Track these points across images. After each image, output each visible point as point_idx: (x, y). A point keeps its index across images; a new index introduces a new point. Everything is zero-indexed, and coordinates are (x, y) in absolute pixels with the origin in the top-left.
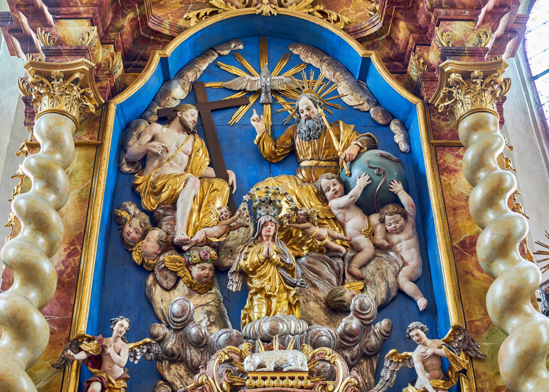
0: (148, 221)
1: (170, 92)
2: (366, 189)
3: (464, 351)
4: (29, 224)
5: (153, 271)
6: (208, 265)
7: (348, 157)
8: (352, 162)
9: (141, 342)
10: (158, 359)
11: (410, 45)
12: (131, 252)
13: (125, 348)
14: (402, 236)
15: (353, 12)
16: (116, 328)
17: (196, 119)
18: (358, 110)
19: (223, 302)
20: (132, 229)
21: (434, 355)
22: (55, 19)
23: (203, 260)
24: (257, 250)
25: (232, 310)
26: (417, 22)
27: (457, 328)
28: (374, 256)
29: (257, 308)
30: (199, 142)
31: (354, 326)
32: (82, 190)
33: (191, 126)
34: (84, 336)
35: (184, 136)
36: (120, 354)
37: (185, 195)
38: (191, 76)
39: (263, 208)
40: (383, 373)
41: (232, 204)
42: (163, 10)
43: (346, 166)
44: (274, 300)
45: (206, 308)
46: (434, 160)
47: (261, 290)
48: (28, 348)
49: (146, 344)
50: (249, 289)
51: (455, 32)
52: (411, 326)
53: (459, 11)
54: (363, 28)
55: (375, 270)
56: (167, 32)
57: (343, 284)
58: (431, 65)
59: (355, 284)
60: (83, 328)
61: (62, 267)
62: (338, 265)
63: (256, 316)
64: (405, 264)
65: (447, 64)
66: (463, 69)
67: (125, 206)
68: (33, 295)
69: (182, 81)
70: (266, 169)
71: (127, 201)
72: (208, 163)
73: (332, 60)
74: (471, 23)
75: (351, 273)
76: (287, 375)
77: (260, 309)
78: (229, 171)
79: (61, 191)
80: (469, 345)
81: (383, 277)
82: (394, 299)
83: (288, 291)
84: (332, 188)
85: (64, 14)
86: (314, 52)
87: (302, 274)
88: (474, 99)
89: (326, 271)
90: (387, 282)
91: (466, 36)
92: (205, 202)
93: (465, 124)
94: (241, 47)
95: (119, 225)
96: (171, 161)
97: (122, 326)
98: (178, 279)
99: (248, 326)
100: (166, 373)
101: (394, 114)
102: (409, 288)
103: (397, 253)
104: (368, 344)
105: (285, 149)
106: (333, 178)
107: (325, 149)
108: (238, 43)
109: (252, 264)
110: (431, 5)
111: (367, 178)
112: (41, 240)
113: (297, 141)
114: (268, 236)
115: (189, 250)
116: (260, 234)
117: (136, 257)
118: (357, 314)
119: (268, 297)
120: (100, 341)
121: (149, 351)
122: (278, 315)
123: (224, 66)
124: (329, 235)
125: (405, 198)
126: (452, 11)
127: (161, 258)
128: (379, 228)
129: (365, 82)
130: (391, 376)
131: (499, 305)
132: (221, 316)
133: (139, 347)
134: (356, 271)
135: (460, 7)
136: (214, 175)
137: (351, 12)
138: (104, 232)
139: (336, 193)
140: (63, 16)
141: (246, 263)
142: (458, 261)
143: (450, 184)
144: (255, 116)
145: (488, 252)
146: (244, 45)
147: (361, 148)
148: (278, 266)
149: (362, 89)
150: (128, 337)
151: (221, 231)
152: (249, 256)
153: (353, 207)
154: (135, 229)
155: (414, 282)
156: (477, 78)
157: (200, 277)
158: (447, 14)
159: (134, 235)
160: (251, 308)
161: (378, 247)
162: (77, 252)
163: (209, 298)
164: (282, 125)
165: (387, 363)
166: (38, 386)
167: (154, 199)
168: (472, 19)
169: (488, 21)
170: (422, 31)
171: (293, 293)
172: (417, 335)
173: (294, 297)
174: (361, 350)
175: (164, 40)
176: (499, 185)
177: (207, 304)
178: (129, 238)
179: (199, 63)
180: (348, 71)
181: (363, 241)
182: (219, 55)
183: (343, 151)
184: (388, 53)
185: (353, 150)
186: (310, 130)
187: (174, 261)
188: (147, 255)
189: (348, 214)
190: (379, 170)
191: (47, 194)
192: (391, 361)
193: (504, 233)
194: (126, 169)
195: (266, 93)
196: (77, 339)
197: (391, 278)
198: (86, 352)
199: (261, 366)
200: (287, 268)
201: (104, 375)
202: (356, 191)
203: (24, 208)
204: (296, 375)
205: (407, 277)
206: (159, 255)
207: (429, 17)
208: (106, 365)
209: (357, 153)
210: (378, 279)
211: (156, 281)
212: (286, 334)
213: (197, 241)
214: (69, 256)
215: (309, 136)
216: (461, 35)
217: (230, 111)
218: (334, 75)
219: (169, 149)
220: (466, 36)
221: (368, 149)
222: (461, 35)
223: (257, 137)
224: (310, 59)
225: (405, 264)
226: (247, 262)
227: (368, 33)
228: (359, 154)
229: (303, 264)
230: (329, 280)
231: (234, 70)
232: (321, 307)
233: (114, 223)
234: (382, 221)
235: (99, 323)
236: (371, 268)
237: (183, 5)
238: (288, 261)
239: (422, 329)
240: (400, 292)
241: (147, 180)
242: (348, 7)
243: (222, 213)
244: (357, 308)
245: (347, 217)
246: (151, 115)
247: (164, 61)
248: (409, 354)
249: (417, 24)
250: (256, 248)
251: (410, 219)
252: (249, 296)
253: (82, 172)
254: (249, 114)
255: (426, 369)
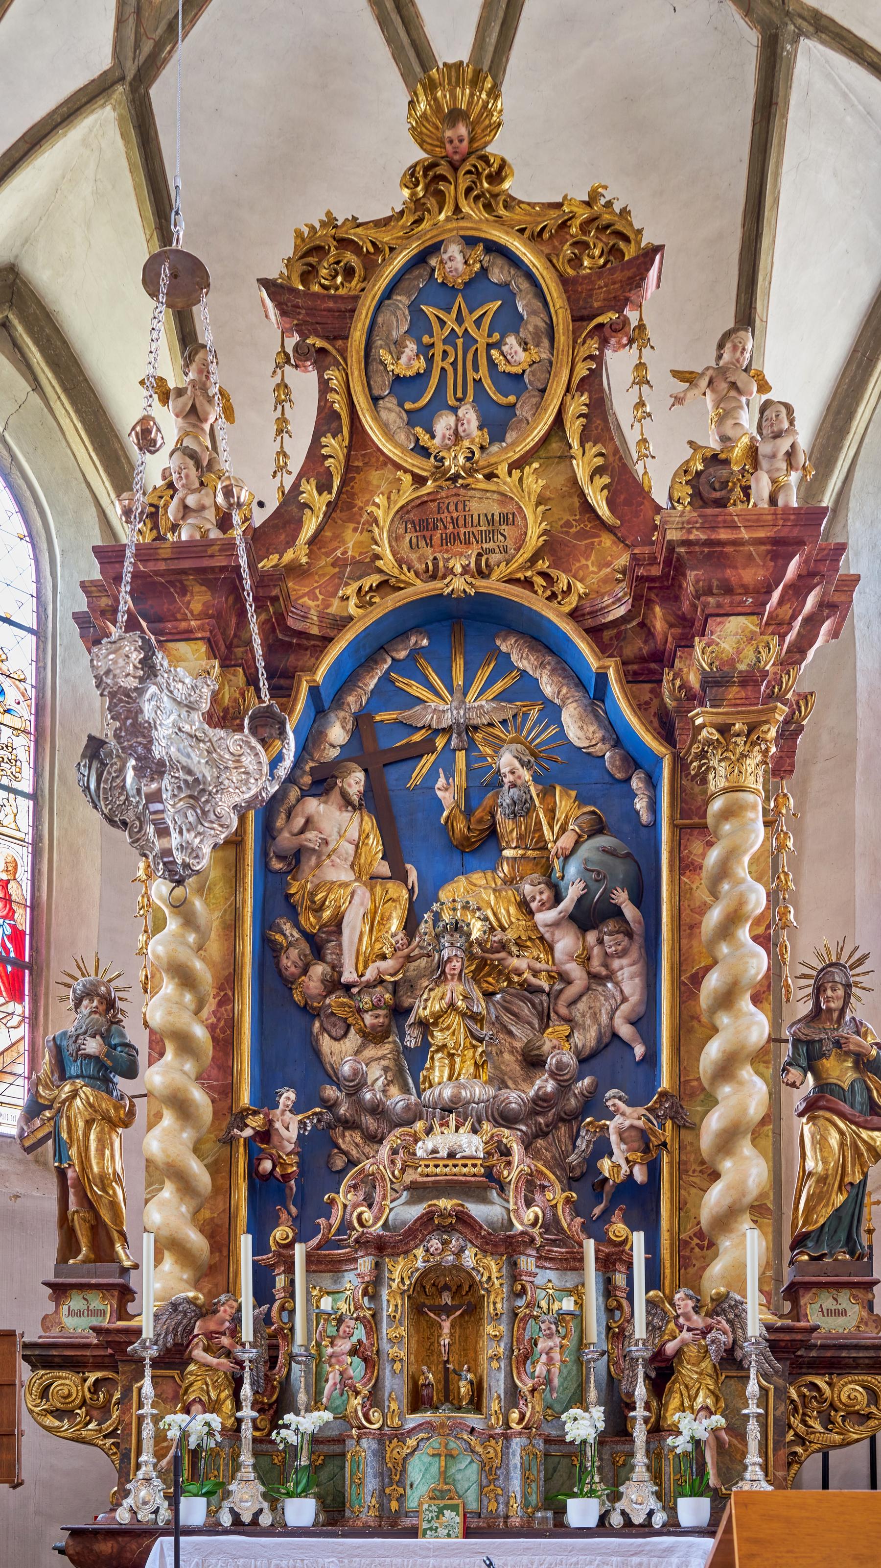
0: (308, 951)
1: (326, 735)
2: (580, 900)
3: (671, 1118)
4: (173, 978)
5: (318, 1015)
6: (382, 1012)
7: (560, 851)
8: (567, 858)
9: (310, 1113)
10: (330, 1126)
11: (668, 645)
12: (291, 989)
13: (294, 1121)
14: (625, 961)
15: (595, 569)
16: (282, 1100)
17: (362, 789)
18: (589, 754)
19: (403, 1053)
20: (290, 961)
21: (632, 1127)
22: (158, 641)
23: (375, 1007)
24: (440, 994)
25: (411, 1064)
26: (680, 609)
27: (664, 1095)
28: (588, 989)
29: (438, 1070)
30: (369, 823)
31: (549, 1089)
32: (225, 911)
33: (355, 799)
34: (248, 1109)
35: (347, 815)
36: (289, 1128)
37: (352, 916)
38: (353, 702)
39: (447, 937)
40: (579, 1142)
41: (410, 926)
42: (307, 582)
43: (557, 864)
44: (458, 1060)
45: (384, 1063)
46: (676, 850)
47: (442, 1048)
48: (193, 1127)
49: (315, 1114)
50: (430, 1045)
51: (723, 645)
52: (607, 1095)
53: (737, 598)
54: (604, 608)
55: (586, 1009)
56: (315, 631)
57: (547, 1026)
58: (691, 688)
59: (561, 1028)
60: (245, 1099)
61: (213, 1020)
62: (542, 1003)
63: (436, 1080)
64: (624, 999)
65: (698, 714)
66: (720, 720)
67: (278, 924)
68: (188, 1066)
69: (342, 714)
70: (457, 859)
71: (281, 916)
72: (380, 855)
73: (558, 663)
74: (755, 617)
75: (556, 1013)
76: (460, 1162)
77: (441, 1072)
78: (409, 866)
79: (202, 928)
80: (677, 1112)
81: (595, 1017)
82: (607, 1046)
83: (475, 1047)
84: (538, 898)
85: (170, 633)
86: (532, 649)
87: (497, 1017)
88: (729, 770)
89: (526, 1010)
90: (599, 1025)
91: (739, 652)
92: (378, 918)
93: (716, 805)
94: (425, 642)
95: (274, 951)
96: (333, 857)
97: (288, 1098)
98: (348, 1026)
99: (428, 1092)
100: (340, 1141)
101: (639, 761)
102: (625, 1031)
103: (617, 984)
104: (567, 1108)
105: (482, 831)
106: (539, 883)
107: (535, 831)
108: (420, 637)
109: (432, 1014)
110: (696, 591)
111: (582, 885)
112: (188, 997)
113: (498, 816)
114: (453, 975)
115: (359, 992)
116: (443, 972)
117: (297, 997)
118: (553, 1075)
119: (451, 1056)
120: (266, 1115)
121: (319, 1121)
122: (462, 1080)
123: (402, 682)
124: (529, 967)
125: (630, 911)
126: (727, 600)
127: (328, 1001)
128: (596, 950)
129: (603, 701)
130: (587, 1146)
131: (709, 1071)
132: (400, 1071)
133: (308, 1118)
134: (563, 1011)
135: (740, 591)
136: (389, 874)
137: (591, 569)
138: (257, 996)
139: (543, 904)
140: (170, 637)
141: (427, 1012)
142: (684, 1002)
143: (691, 889)
144: (441, 782)
145: (710, 1002)
146: (429, 639)
147: (580, 836)
148: (463, 1015)
149: (597, 716)
150: (296, 1109)
151: (398, 966)
152: (429, 1004)
153: (565, 923)
154: (294, 962)
155: (632, 1024)
156: (738, 735)
157: (373, 1026)
158: (719, 605)
159: (293, 969)
160: (432, 1068)
161: (594, 977)
162: (229, 999)
163: (386, 1049)
164: (484, 783)
165: (583, 1133)
166: (206, 1162)
167: (315, 917)
168: (756, 611)
169: (789, 600)
170: (686, 623)
171: (480, 1050)
172: (614, 1105)
173: (481, 1055)
174: (559, 1114)
175: (312, 643)
176: (736, 911)
177: (383, 1057)
178: (287, 973)
179: (364, 677)
180: (580, 684)
181: (575, 970)
182: (393, 659)
183: (555, 842)
184: (640, 649)
185: (567, 841)
186: (515, 803)
187: (343, 1005)
188: (312, 998)
189: (558, 934)
190: (599, 873)
191: (187, 935)
192: (588, 1131)
193: (729, 980)
194: (277, 865)
195: (459, 734)
196: (241, 1112)
197: (604, 1019)
198: (253, 1128)
199: (435, 1151)
200: (476, 1018)
201: (274, 1152)
202: (573, 893)
203: (165, 960)
204: (469, 1162)
205: (625, 1018)
206: (325, 997)
207: (695, 607)
208: (275, 1139)
209: (572, 844)
210: (589, 1022)
211: (323, 1029)
212: (469, 1103)
213: (368, 981)
214: (220, 1004)
215: (513, 812)
216: (731, 650)
217: (410, 763)
218: (559, 693)
219: (329, 839)
220: (739, 652)
221: (589, 837)
222: (731, 650)
223: (445, 814)
224: (525, 662)
225: (624, 999)
226: (427, 1012)
227: (611, 617)
228: (577, 844)
229: (498, 1002)
230: (530, 1024)
231: (417, 690)
232: (517, 1060)
233: (268, 950)
234: (600, 941)
235: (262, 1081)
236: (582, 1006)
237: (337, 570)
238: (475, 1009)
239: (620, 1098)
240: (615, 1035)
241: (304, 887)
242: (587, 560)
243: (397, 942)
244: (553, 1068)
245: (556, 937)
246: (302, 777)
247: (314, 691)
248: (608, 1123)
249: (680, 613)
250: (438, 991)
251: (635, 937)
252: (430, 1054)
253: (221, 884)
254: (432, 775)
255: (622, 1139)
